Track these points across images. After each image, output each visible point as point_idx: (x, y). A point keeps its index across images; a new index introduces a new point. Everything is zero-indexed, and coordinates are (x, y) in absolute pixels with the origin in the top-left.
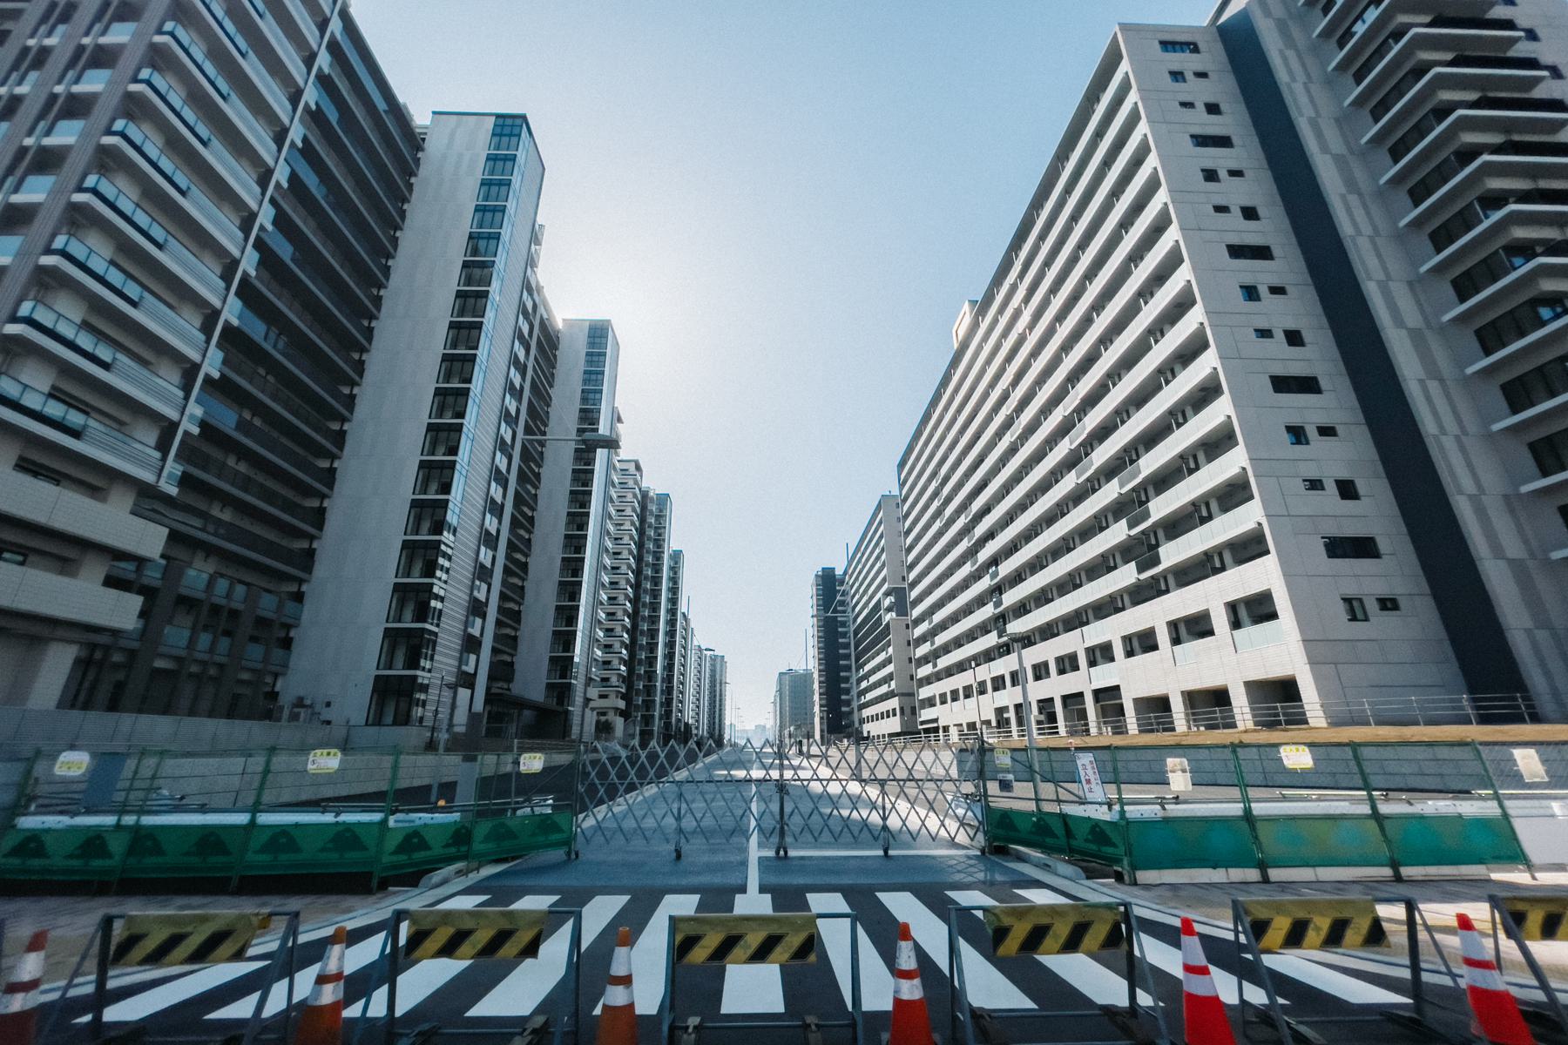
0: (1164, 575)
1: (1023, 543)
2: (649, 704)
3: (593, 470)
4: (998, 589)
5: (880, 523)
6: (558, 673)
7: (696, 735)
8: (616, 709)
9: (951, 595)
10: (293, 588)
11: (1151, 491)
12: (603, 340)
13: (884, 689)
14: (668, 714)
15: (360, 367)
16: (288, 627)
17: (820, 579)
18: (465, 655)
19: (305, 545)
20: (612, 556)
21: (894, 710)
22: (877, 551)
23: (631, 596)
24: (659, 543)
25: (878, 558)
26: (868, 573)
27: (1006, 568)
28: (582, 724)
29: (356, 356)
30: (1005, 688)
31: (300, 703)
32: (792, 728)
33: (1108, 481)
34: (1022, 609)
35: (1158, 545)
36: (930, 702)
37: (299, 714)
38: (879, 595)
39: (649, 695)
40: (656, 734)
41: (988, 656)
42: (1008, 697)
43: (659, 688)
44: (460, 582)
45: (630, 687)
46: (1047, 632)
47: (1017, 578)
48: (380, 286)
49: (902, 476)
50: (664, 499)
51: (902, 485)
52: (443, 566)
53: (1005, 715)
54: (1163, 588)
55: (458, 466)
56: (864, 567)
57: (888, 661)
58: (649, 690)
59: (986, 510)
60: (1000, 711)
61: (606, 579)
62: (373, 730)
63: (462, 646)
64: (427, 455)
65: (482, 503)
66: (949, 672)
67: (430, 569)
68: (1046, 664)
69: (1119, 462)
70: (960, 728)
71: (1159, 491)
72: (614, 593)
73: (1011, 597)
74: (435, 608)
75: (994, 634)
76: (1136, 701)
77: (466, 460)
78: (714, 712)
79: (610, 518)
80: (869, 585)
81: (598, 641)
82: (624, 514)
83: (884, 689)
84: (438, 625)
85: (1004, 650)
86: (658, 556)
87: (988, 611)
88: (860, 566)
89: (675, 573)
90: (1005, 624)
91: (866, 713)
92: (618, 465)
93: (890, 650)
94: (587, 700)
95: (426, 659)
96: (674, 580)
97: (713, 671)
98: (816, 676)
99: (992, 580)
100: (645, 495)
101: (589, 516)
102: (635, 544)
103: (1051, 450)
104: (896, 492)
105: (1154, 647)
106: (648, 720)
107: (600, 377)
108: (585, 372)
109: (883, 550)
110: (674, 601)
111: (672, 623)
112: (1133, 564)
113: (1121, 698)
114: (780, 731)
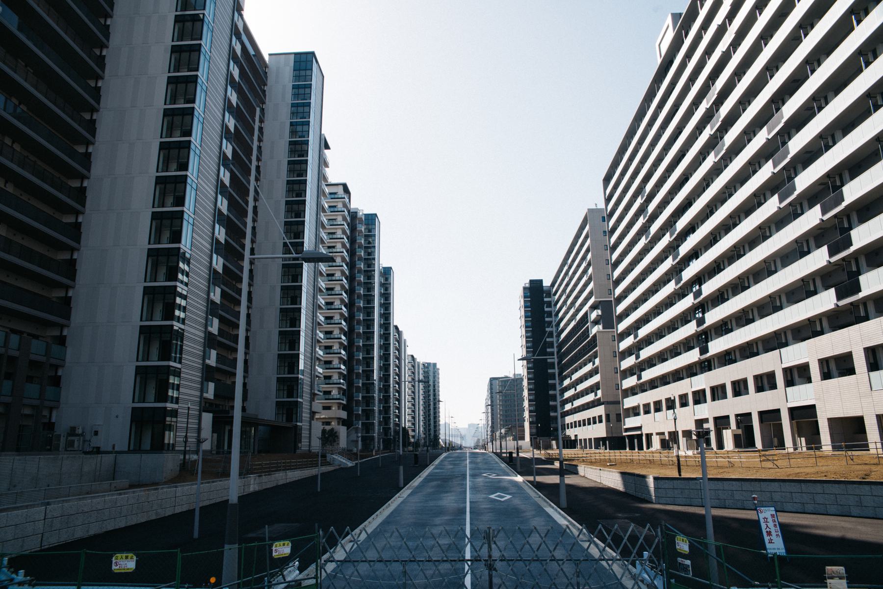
0: (865, 301)
1: (726, 263)
2: (368, 414)
3: (305, 201)
4: (703, 306)
5: (586, 237)
6: (286, 369)
7: (413, 437)
8: (339, 419)
9: (657, 311)
10: (56, 333)
11: (854, 218)
12: (308, 73)
13: (590, 397)
14: (387, 420)
15: (92, 127)
16: (56, 367)
17: (528, 291)
18: (205, 383)
19: (62, 294)
20: (324, 366)
21: (600, 417)
22: (584, 265)
23: (346, 315)
24: (370, 261)
25: (585, 271)
26: (576, 285)
27: (709, 287)
28: (310, 437)
29: (87, 116)
30: (706, 402)
31: (72, 432)
32: (503, 431)
33: (811, 207)
34: (724, 327)
35: (859, 273)
36: (634, 411)
37: (73, 441)
38: (586, 308)
39: (368, 392)
40: (376, 440)
41: (691, 371)
42: (708, 410)
43: (377, 399)
44: (195, 321)
45: (350, 398)
46: (748, 350)
47: (720, 297)
48: (103, 46)
49: (608, 191)
50: (371, 219)
51: (608, 200)
52: (180, 305)
53: (705, 426)
54: (862, 314)
55: (186, 216)
56: (571, 279)
57: (594, 372)
58: (368, 400)
59: (691, 228)
60: (700, 423)
61: (322, 301)
62: (135, 458)
63: (202, 377)
64: (158, 207)
65: (209, 247)
66: (653, 384)
67: (169, 314)
68: (745, 381)
69: (822, 187)
70: (662, 437)
71: (863, 219)
72: (330, 313)
73: (713, 316)
74: (173, 384)
75: (696, 351)
76: (832, 422)
77: (192, 209)
78: (429, 410)
79: (322, 242)
80: (577, 298)
81: (319, 342)
82: (335, 236)
83: (590, 397)
84: (180, 362)
85: (705, 366)
86: (369, 274)
87: (690, 329)
88: (567, 279)
89: (387, 279)
90: (707, 342)
91: (569, 419)
92: (327, 190)
93: (597, 361)
94: (313, 414)
95: (173, 389)
96: (386, 296)
97: (426, 381)
98: (525, 383)
99: (695, 298)
100: (354, 215)
101: (307, 163)
102: (347, 265)
103: (813, 71)
104: (602, 205)
105: (851, 371)
106: (368, 427)
107: (307, 91)
108: (293, 105)
109: (589, 265)
110: (386, 316)
111: (385, 336)
112: (833, 290)
113: (817, 417)
114: (493, 431)
